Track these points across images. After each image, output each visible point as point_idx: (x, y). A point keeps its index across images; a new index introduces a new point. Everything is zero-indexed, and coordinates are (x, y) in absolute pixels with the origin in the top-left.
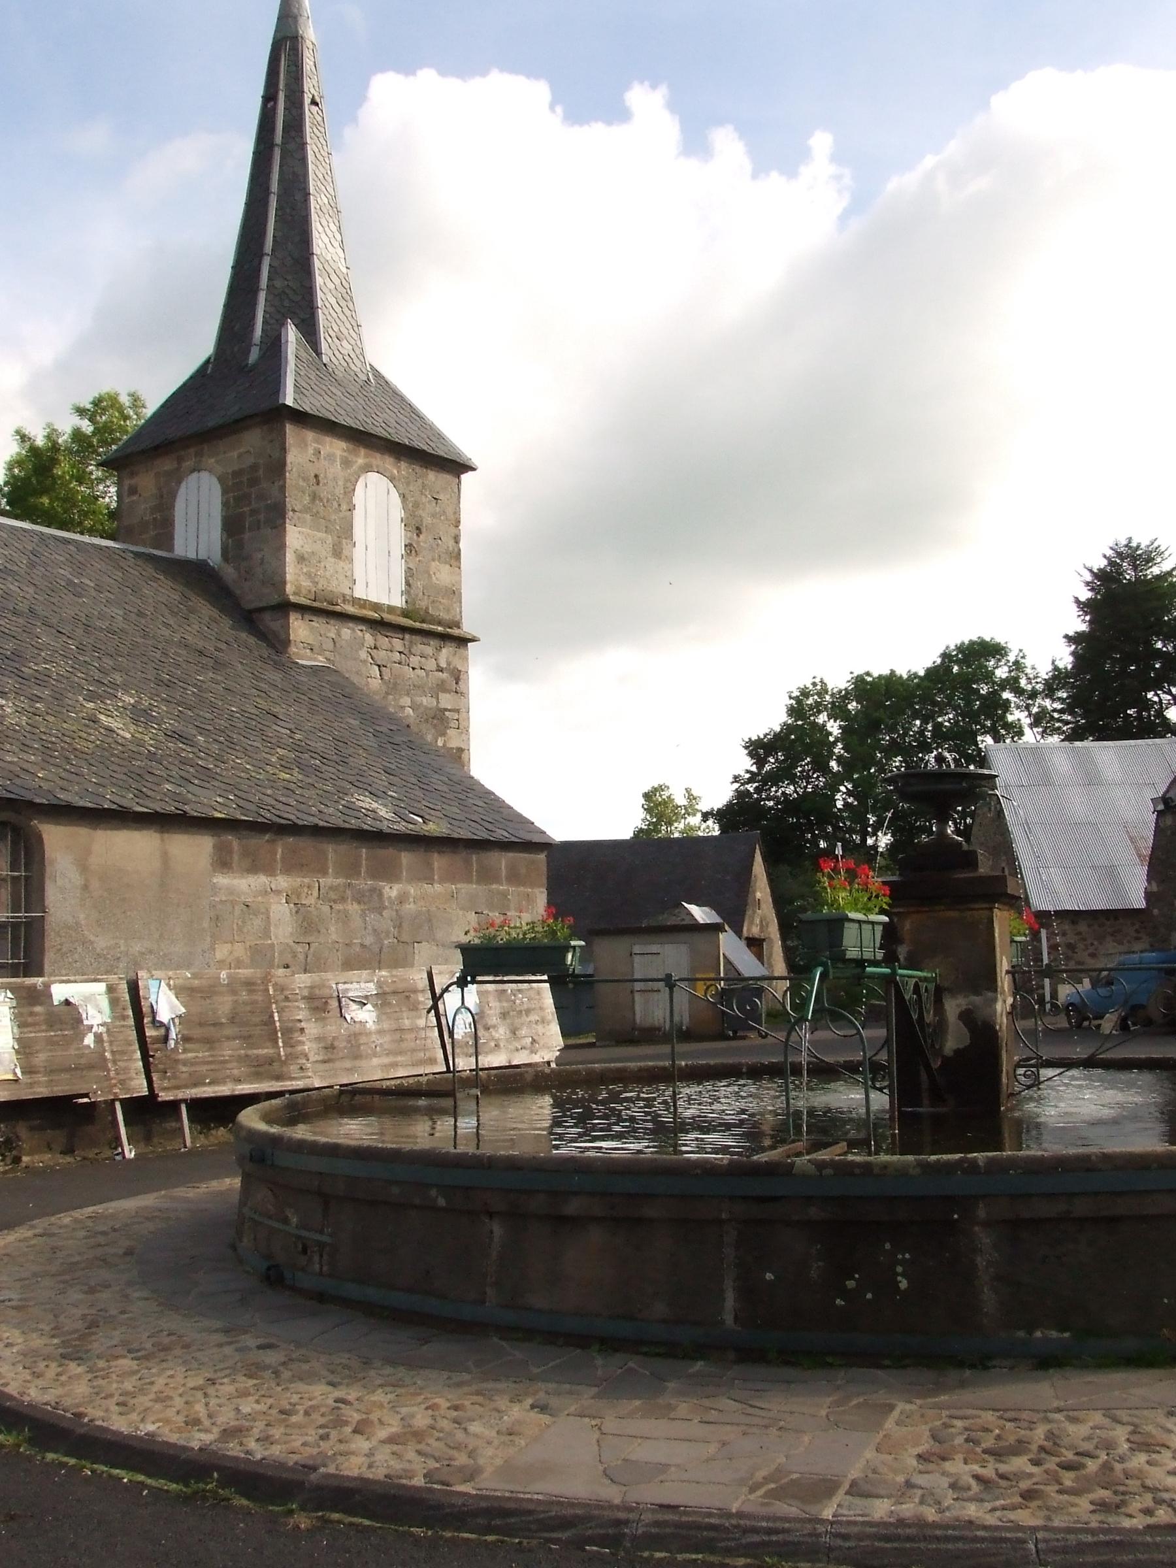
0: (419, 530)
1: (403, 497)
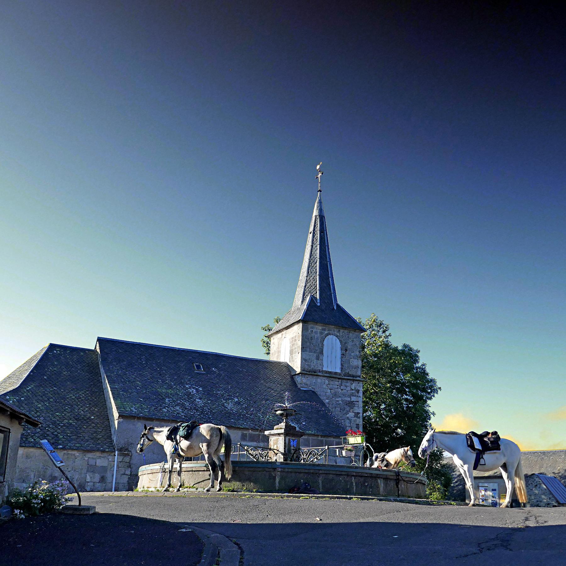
0: (346, 350)
1: (341, 341)
